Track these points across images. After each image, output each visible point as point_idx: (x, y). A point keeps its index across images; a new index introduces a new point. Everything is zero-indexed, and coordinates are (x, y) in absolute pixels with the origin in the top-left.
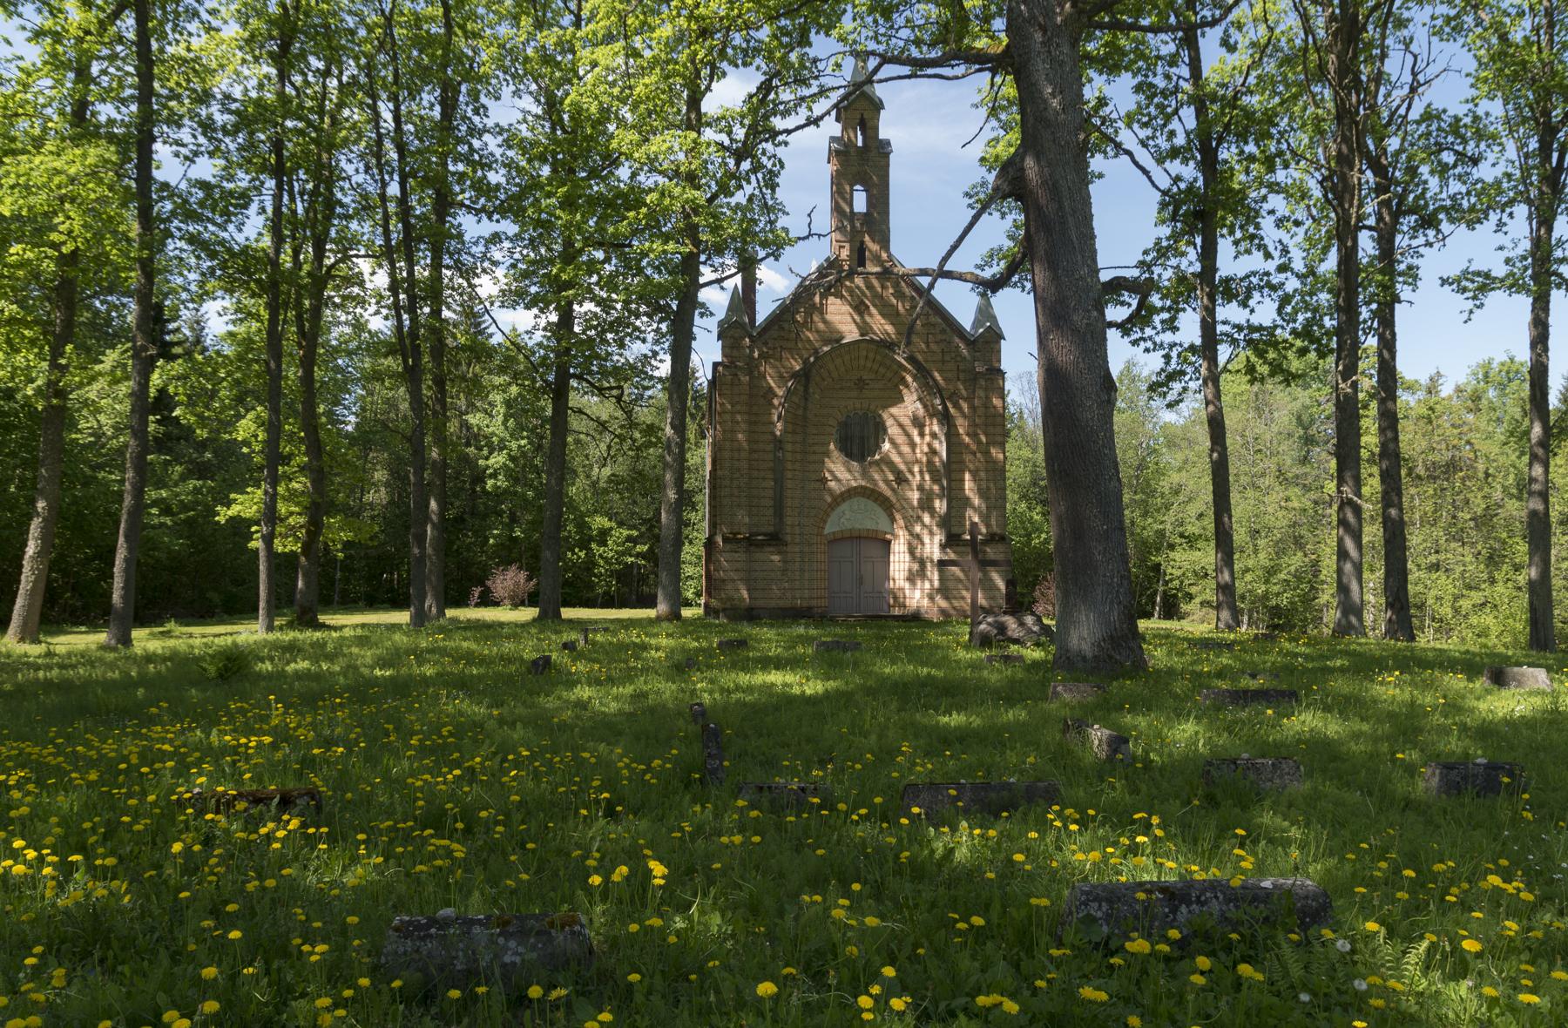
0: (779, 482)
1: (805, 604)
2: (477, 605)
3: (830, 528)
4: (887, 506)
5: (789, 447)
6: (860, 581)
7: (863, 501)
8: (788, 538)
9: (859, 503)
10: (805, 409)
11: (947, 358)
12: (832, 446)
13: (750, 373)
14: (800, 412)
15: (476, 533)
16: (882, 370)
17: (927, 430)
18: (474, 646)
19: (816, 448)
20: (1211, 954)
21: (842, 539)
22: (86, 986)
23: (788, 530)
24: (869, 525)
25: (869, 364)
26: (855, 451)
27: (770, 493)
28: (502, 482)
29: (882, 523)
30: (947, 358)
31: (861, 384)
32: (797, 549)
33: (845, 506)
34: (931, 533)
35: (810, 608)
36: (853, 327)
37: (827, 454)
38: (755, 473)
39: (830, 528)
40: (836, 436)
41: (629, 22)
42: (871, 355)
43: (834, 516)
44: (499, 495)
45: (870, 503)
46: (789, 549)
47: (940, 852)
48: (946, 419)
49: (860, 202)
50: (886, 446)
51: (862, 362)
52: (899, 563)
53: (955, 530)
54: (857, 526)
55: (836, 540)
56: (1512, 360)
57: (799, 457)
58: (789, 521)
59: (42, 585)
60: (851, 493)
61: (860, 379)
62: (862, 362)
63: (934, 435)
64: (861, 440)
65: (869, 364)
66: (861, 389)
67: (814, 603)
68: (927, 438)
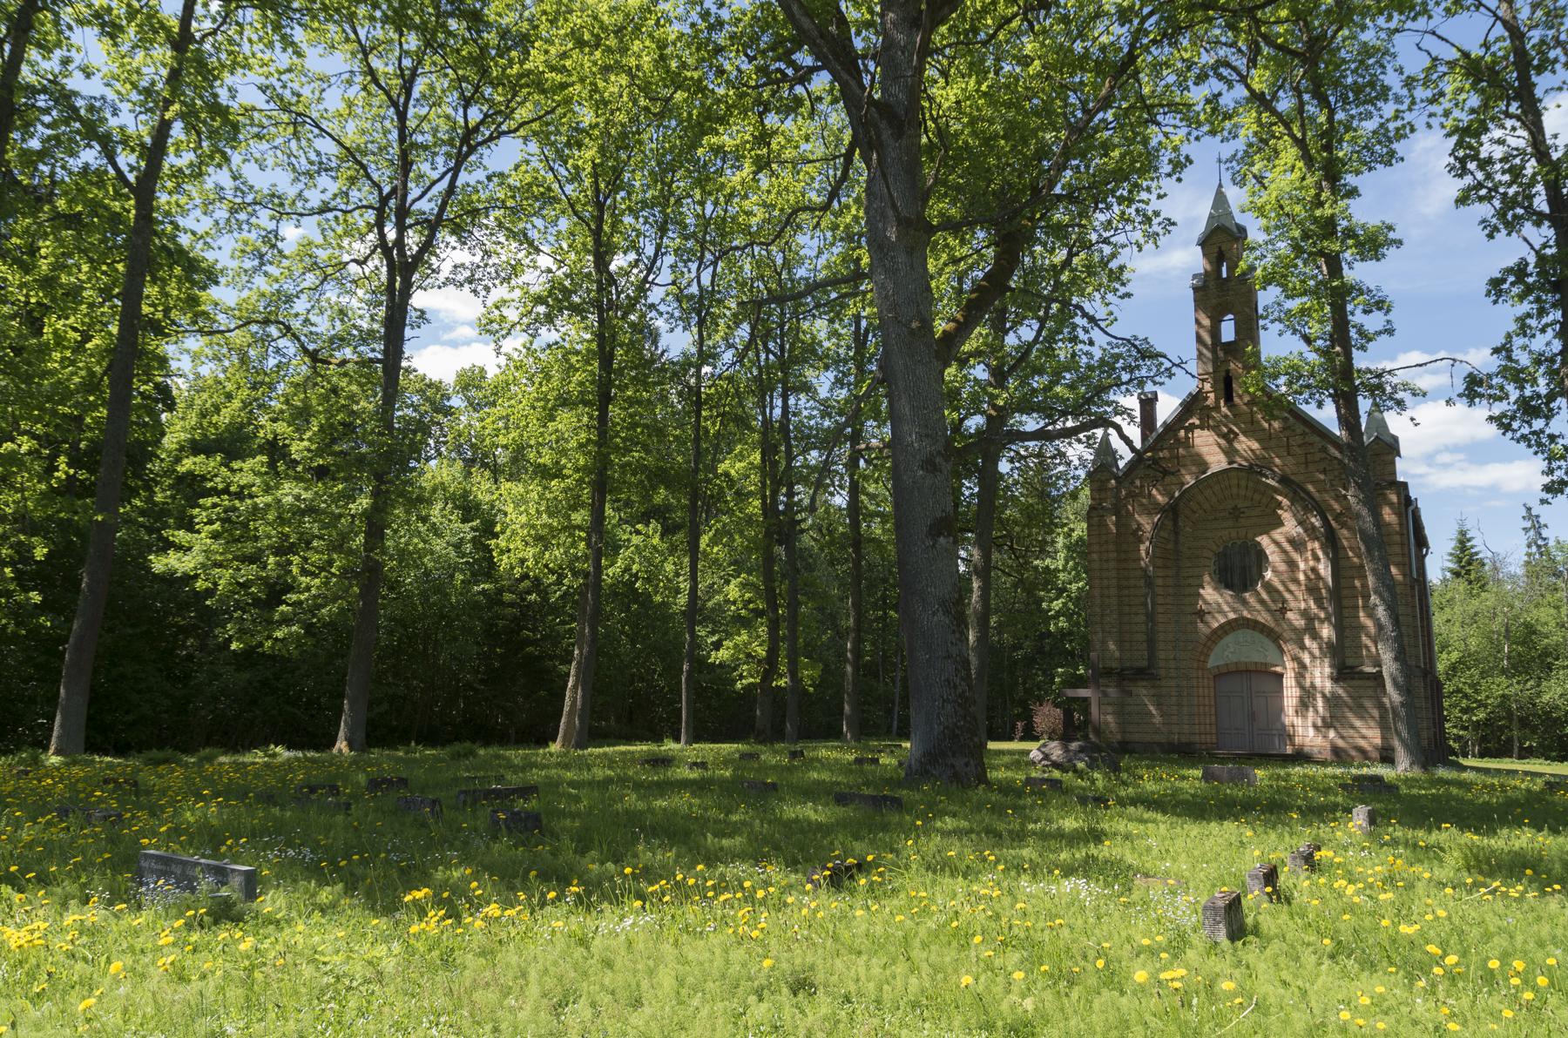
0: (1151, 617)
1: (1184, 739)
2: (1022, 739)
3: (1212, 662)
4: (1274, 637)
5: (1160, 582)
6: (1252, 716)
7: (1257, 634)
8: (1162, 672)
9: (1244, 635)
10: (1176, 542)
13: (1117, 514)
14: (1171, 546)
15: (1044, 673)
16: (1257, 497)
18: (839, 756)
19: (1190, 581)
21: (1229, 673)
23: (1161, 664)
24: (1257, 658)
25: (1242, 492)
26: (1236, 581)
27: (1143, 628)
28: (1063, 623)
29: (1271, 655)
31: (1236, 513)
32: (1173, 683)
33: (1228, 639)
35: (1189, 744)
36: (1222, 457)
38: (1126, 609)
39: (1212, 662)
40: (1213, 567)
42: (1243, 483)
43: (1217, 650)
44: (1063, 635)
46: (1163, 683)
48: (1331, 543)
49: (1228, 331)
50: (1268, 575)
51: (1235, 490)
53: (1350, 662)
54: (1243, 659)
55: (1221, 675)
57: (1171, 590)
58: (1162, 655)
60: (1230, 627)
61: (1236, 508)
62: (1235, 490)
64: (1240, 570)
65: (1242, 492)
66: (1237, 518)
67: (1196, 739)
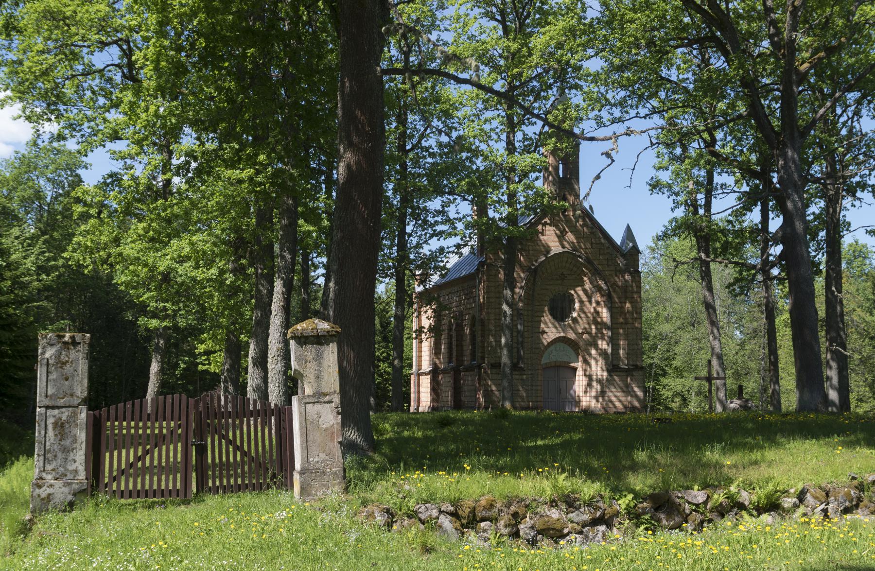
3: (544, 361)
9: (561, 345)
11: (610, 263)
12: (546, 309)
16: (575, 269)
17: (593, 300)
20: (516, 326)
22: (36, 78)
30: (610, 263)
34: (597, 361)
37: (543, 311)
39: (544, 361)
41: (411, 59)
42: (570, 261)
43: (546, 355)
45: (566, 346)
47: (517, 456)
52: (580, 383)
55: (548, 367)
56: (857, 242)
59: (92, 419)
61: (562, 274)
63: (598, 303)
68: (594, 305)
